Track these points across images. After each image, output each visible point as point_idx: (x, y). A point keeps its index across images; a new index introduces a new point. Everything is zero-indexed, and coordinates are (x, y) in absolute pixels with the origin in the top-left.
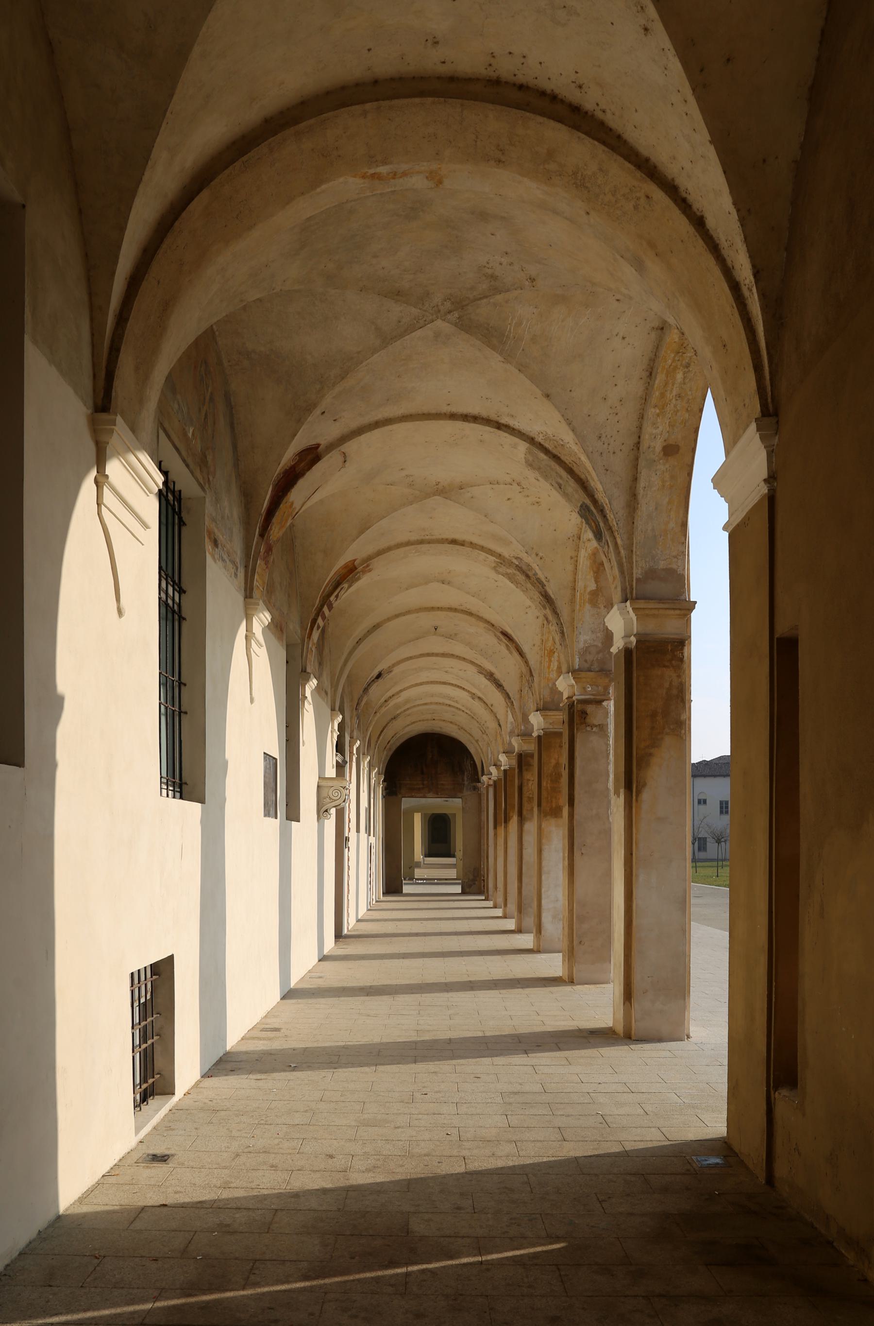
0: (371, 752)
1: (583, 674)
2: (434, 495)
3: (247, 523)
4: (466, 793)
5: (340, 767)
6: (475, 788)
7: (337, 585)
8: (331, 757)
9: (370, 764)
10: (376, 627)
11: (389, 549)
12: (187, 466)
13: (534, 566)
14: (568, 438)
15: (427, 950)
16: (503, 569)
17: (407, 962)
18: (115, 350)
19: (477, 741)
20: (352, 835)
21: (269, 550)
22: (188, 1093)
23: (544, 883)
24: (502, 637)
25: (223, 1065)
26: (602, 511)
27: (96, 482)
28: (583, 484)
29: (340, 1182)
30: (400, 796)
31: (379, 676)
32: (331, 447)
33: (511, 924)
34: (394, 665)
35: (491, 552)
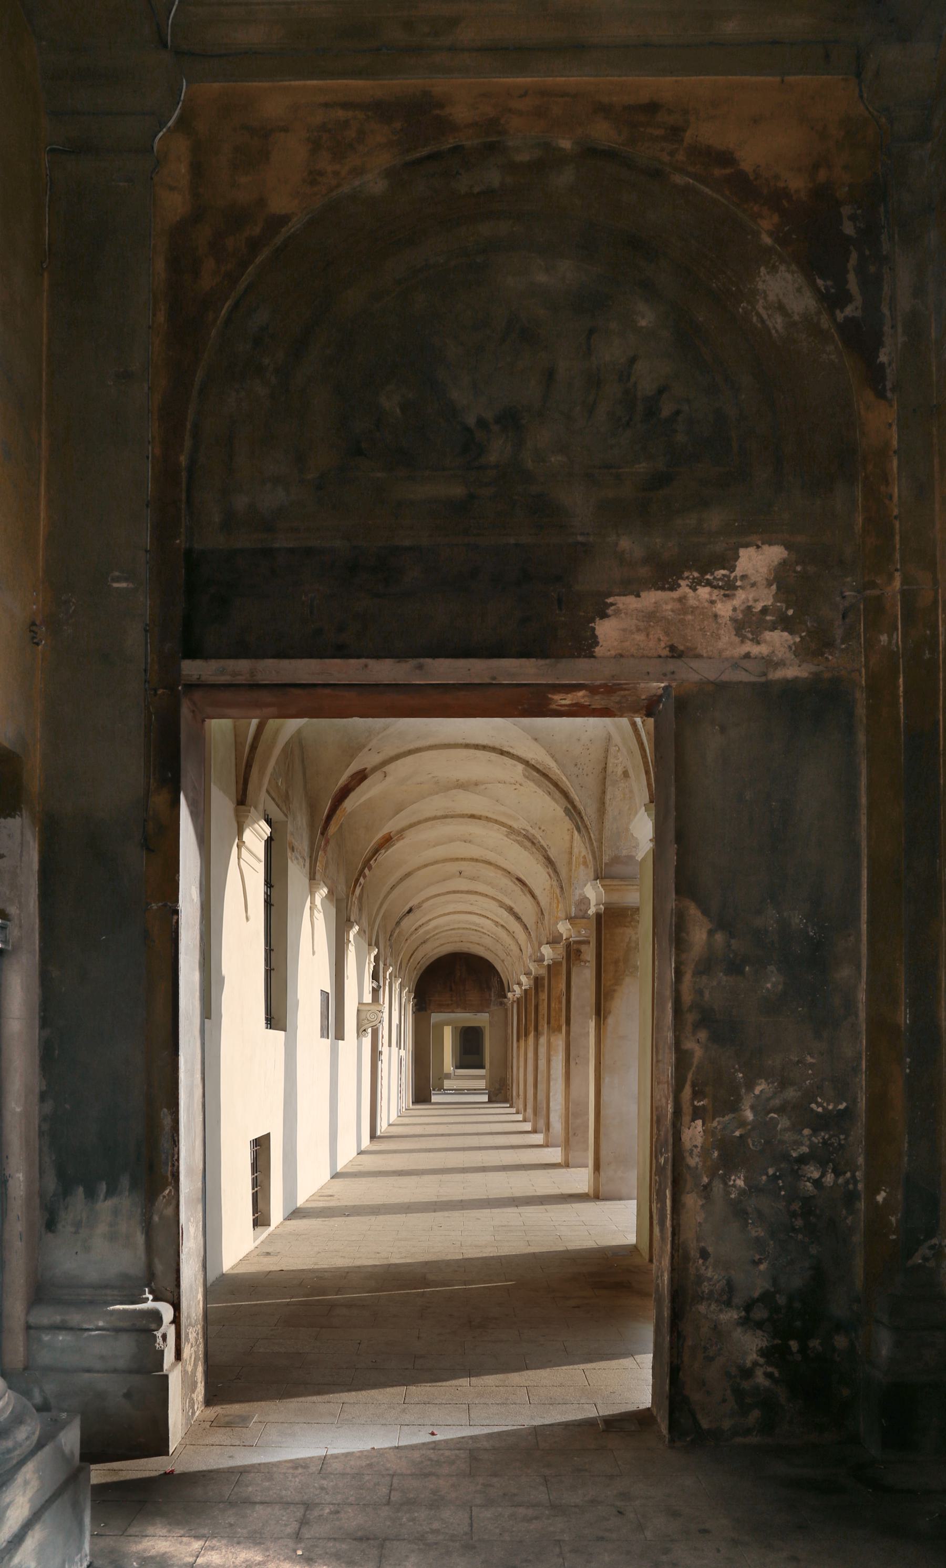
0: (402, 973)
1: (578, 921)
2: (455, 788)
3: (312, 826)
4: (493, 1008)
5: (375, 991)
6: (501, 1004)
7: (376, 851)
8: (368, 984)
9: (402, 986)
10: (408, 875)
11: (419, 822)
12: (278, 806)
13: (538, 836)
14: (553, 765)
15: (450, 1146)
16: (513, 837)
17: (432, 1154)
18: (249, 766)
19: (503, 961)
20: (385, 1049)
21: (327, 842)
22: (278, 1227)
23: (552, 1088)
24: (517, 882)
25: (295, 1214)
26: (579, 814)
27: (238, 846)
28: (565, 795)
29: (386, 1262)
30: (429, 1011)
31: (410, 911)
32: (375, 769)
33: (528, 1126)
34: (423, 902)
35: (503, 824)
